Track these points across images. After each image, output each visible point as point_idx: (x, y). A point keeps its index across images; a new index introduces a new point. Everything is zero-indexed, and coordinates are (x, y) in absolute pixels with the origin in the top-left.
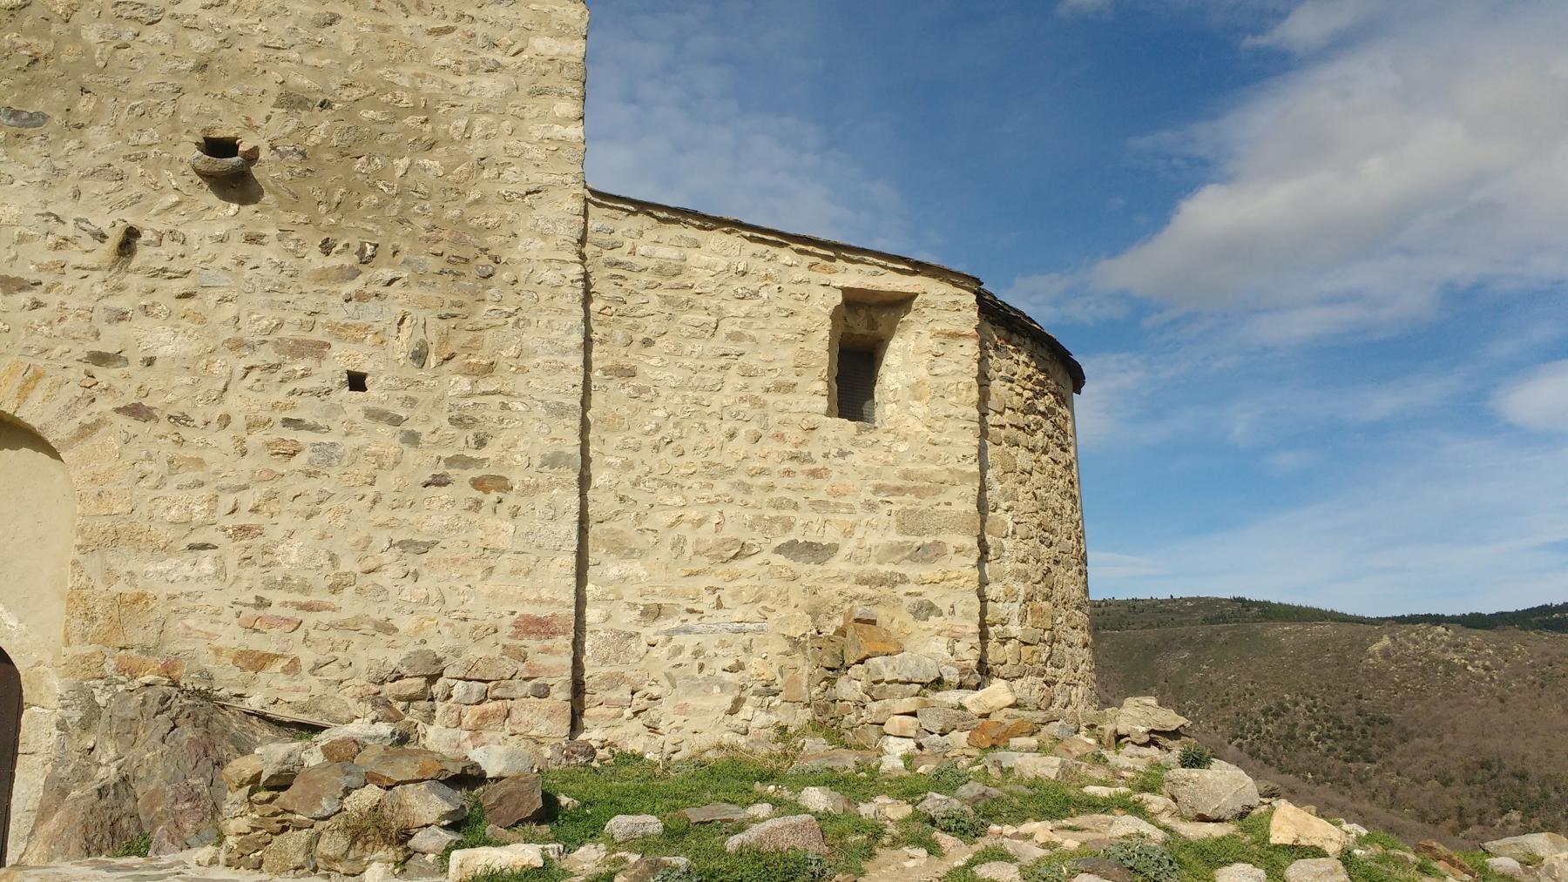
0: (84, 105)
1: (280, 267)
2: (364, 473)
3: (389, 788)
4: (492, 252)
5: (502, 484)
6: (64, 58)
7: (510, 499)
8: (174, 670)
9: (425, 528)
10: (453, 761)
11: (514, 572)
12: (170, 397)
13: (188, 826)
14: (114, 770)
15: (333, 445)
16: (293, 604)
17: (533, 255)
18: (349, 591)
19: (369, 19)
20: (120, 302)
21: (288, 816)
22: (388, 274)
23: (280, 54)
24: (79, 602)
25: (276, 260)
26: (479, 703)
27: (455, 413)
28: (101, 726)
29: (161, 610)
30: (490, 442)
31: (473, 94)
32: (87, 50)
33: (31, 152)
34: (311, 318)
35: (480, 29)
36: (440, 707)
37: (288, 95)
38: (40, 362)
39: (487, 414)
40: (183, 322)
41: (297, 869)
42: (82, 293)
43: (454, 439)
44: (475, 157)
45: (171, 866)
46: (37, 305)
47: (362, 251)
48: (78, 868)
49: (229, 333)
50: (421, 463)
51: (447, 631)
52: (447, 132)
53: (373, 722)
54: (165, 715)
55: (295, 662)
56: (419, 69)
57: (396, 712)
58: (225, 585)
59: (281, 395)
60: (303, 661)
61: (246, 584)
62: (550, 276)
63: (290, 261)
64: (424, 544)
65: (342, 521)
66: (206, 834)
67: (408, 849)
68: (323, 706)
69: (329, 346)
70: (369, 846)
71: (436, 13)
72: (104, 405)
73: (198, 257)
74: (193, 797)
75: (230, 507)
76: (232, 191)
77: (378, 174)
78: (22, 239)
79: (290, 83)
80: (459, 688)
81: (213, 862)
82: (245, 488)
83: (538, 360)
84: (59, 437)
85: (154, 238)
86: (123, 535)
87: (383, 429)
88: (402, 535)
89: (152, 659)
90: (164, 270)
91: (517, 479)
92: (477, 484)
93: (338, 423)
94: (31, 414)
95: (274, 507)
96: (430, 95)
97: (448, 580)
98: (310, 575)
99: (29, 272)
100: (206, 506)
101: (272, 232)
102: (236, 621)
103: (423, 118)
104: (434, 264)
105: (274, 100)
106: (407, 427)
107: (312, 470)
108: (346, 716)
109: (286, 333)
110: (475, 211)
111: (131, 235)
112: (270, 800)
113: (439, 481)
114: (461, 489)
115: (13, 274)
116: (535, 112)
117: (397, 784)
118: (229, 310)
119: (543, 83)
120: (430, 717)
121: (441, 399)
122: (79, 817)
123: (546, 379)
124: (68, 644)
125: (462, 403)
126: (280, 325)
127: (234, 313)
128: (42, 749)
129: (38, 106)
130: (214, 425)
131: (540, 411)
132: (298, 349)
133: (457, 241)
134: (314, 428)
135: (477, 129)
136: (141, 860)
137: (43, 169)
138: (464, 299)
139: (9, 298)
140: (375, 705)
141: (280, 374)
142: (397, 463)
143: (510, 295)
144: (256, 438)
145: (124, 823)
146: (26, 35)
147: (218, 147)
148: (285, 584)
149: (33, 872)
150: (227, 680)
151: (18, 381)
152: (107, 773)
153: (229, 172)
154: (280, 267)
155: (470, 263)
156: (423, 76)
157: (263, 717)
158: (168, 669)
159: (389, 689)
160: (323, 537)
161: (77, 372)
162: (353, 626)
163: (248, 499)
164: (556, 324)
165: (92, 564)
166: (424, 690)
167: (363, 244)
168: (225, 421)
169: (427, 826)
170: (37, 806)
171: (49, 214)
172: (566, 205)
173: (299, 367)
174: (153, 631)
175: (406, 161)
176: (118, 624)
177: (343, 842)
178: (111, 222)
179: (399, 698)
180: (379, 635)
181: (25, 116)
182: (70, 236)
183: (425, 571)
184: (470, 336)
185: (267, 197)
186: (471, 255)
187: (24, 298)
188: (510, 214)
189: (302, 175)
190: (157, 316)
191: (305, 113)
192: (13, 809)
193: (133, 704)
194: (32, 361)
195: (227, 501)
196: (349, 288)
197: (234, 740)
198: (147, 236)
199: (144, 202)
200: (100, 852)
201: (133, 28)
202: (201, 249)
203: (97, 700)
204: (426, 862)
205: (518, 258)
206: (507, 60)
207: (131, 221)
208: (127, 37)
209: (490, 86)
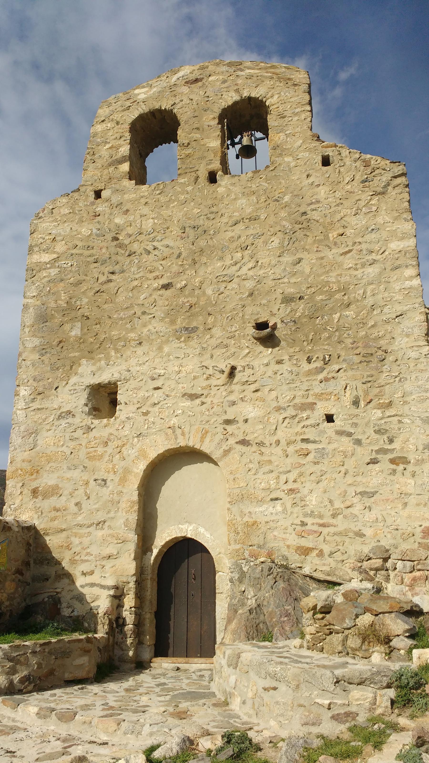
0: (210, 320)
1: (291, 372)
2: (339, 460)
3: (376, 615)
4: (383, 348)
5: (405, 461)
6: (201, 303)
7: (410, 468)
8: (272, 555)
9: (371, 485)
10: (406, 603)
11: (418, 505)
12: (256, 435)
13: (287, 628)
14: (254, 601)
15: (323, 449)
16: (317, 524)
17: (403, 346)
18: (340, 517)
19: (314, 256)
20: (232, 398)
21: (332, 627)
22: (337, 367)
23: (280, 281)
24: (231, 524)
25: (289, 369)
26: (411, 572)
27: (377, 428)
28: (246, 581)
29: (263, 528)
30: (395, 440)
31: (365, 277)
32: (209, 298)
33: (193, 343)
34: (307, 393)
35: (364, 246)
36: (392, 574)
37: (285, 298)
38: (207, 427)
39: (392, 426)
40: (257, 402)
41: (339, 653)
42: (218, 396)
43: (377, 440)
44: (369, 306)
45: (283, 647)
46: (203, 403)
47: (324, 359)
48: (246, 646)
49: (275, 404)
50: (364, 453)
51: (389, 536)
52: (355, 297)
53: (361, 581)
54: (271, 576)
55: (321, 551)
56: (339, 272)
57: (371, 576)
58: (288, 516)
59: (298, 429)
60: (325, 551)
61: (296, 515)
62: (413, 354)
63: (295, 369)
64: (371, 493)
65: (332, 484)
66: (295, 633)
67: (390, 647)
68: (337, 573)
69: (316, 404)
70: (371, 644)
71: (343, 245)
72: (232, 441)
73: (259, 374)
74: (288, 615)
75: (285, 481)
76: (268, 343)
77: (327, 323)
78: (195, 378)
79: (286, 292)
80: (400, 564)
81: (301, 647)
82: (289, 471)
83: (413, 397)
84: (217, 456)
85: (242, 369)
86: (245, 496)
87: (345, 439)
88: (360, 489)
89: (263, 551)
90: (247, 381)
91: (412, 457)
92: (392, 461)
93: (324, 438)
94: (206, 448)
95: (303, 479)
96: (345, 283)
97: (385, 510)
98: (322, 510)
99: (198, 391)
100: (275, 481)
101: (286, 357)
102: (294, 532)
103: (343, 293)
104: (357, 359)
105: (280, 301)
106: (355, 437)
107: (316, 461)
108: (348, 578)
109: (297, 401)
110: (373, 330)
111: (233, 368)
112: (323, 618)
113: (374, 462)
114: (385, 465)
115: (193, 392)
116: (395, 278)
117: (380, 613)
118: (274, 394)
119: (398, 263)
120: (387, 579)
121: (369, 422)
122: (243, 623)
123: (419, 406)
124: (230, 545)
125: (379, 422)
126: (294, 397)
127: (276, 395)
128: (225, 591)
129: (194, 324)
130: (274, 445)
131: (419, 422)
132: (303, 407)
133: (366, 346)
134: (314, 442)
135: (369, 293)
136: (270, 644)
137: (199, 349)
138: (373, 372)
139: (193, 402)
140: (361, 573)
141: (297, 419)
142: (353, 454)
143: (395, 368)
144: (291, 449)
145: (261, 625)
146: (187, 297)
147: (261, 326)
148: (312, 514)
149: (229, 647)
150: (294, 560)
151: (200, 435)
152: (251, 603)
153: (266, 334)
154: (291, 372)
155: (374, 355)
156: (341, 275)
157: (311, 578)
158: (269, 555)
159: (366, 565)
160: (325, 492)
161: (220, 429)
162: (344, 534)
163: (292, 477)
164: (420, 378)
165: (235, 509)
166: (383, 565)
167: (324, 356)
168: (278, 442)
169: (398, 636)
170: (226, 616)
171: (203, 366)
172: (417, 319)
173: (305, 415)
174: (261, 537)
175: (338, 314)
176: (248, 535)
177: (359, 641)
178: (225, 365)
179: (371, 569)
180: (357, 538)
181: (190, 329)
182: (211, 374)
183: (374, 506)
184: (378, 390)
185: (283, 343)
186: (373, 352)
187: (198, 401)
188: (389, 328)
189: (296, 331)
190: (246, 401)
191: (293, 304)
192: (217, 617)
193: (257, 571)
194: (204, 426)
195: (283, 478)
196: (321, 376)
197: (301, 588)
198: (239, 368)
199: (236, 354)
200: (253, 639)
201: (224, 285)
202: (260, 370)
203: (244, 569)
204: (400, 654)
205: (396, 349)
206: (379, 257)
207: (233, 363)
208: (222, 289)
209: (372, 271)
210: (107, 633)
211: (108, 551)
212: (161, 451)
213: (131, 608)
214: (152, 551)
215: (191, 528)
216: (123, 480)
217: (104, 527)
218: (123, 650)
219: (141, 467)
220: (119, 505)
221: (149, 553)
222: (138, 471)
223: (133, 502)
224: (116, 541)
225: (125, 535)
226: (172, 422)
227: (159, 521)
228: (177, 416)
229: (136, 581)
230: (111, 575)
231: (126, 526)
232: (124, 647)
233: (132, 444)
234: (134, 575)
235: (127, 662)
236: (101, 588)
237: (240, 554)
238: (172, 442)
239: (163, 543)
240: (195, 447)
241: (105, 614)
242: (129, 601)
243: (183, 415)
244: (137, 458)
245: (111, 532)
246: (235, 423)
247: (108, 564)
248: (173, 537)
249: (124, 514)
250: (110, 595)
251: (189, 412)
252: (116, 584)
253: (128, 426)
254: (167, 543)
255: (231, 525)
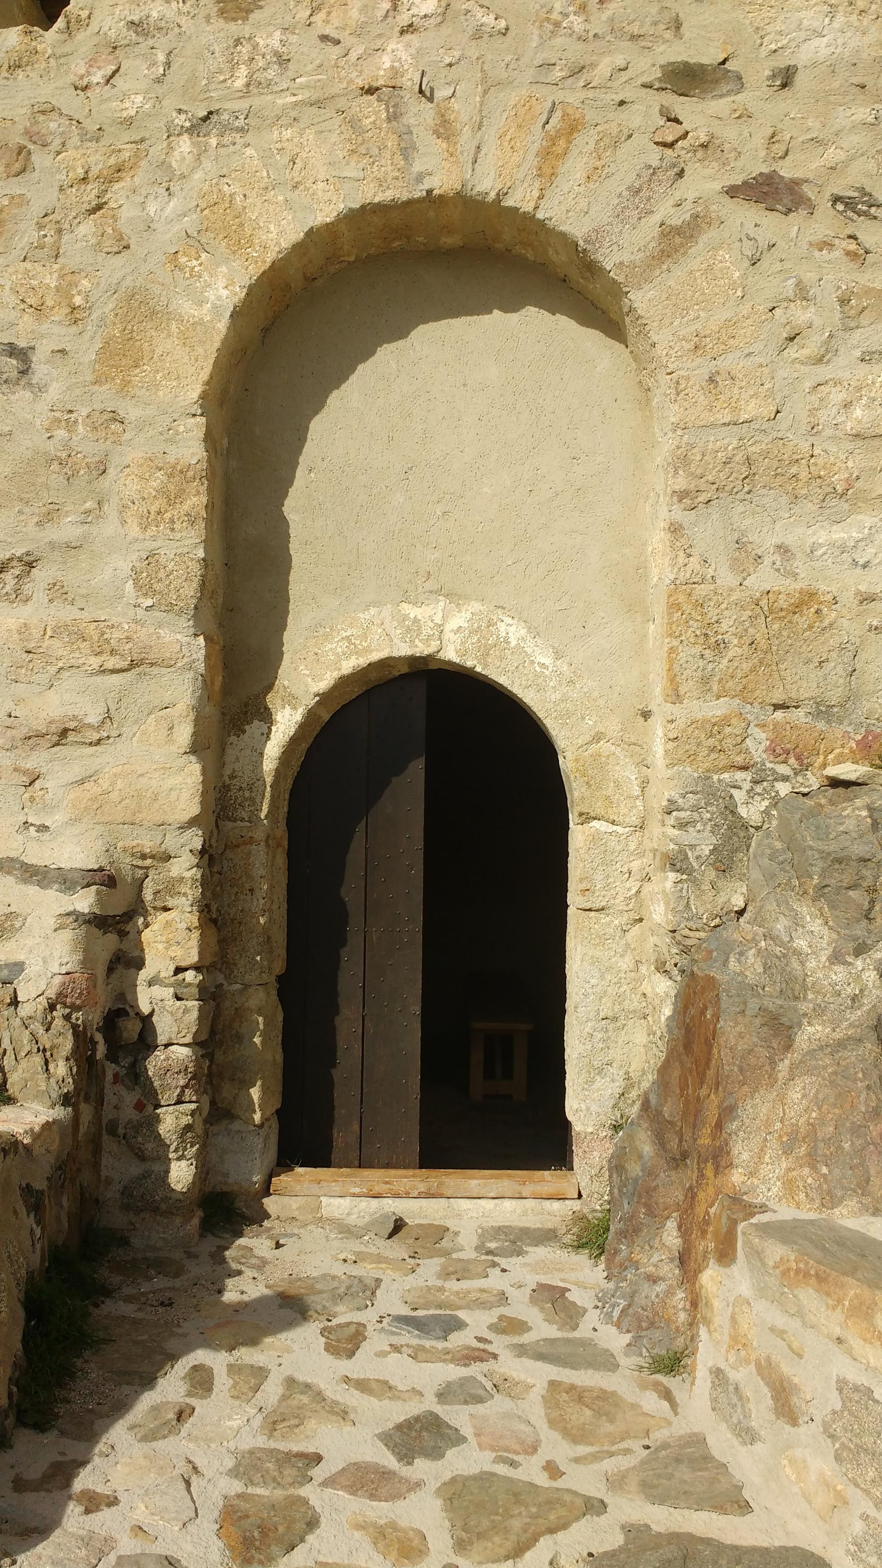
12: (833, 155)
29: (849, 628)
38: (573, 97)
72: (704, 182)
84: (626, 257)
89: (838, 730)
94: (572, 206)
151: (535, 140)
165: (708, 531)
174: (836, 670)
203: (743, 811)
210: (66, 1100)
211: (53, 705)
212: (325, 215)
213: (179, 970)
214: (267, 717)
215: (459, 620)
216: (121, 357)
217: (27, 588)
218: (143, 1158)
219: (218, 292)
220: (106, 482)
221: (255, 727)
222: (204, 312)
223: (177, 472)
224: (95, 662)
225: (143, 634)
226: (386, 61)
227: (298, 586)
228: (408, 29)
229: (203, 852)
230: (77, 820)
231: (144, 588)
232: (150, 1146)
233: (164, 165)
234: (193, 822)
235: (169, 1213)
236: (25, 881)
237: (729, 743)
238: (387, 166)
239: (324, 684)
240: (509, 202)
241: (52, 1007)
242: (170, 941)
243: (445, 30)
244: (194, 241)
245: (66, 614)
246: (724, 88)
247: (61, 769)
248: (375, 656)
249: (134, 530)
250: (75, 915)
251: (479, 13)
252: (104, 862)
253: (137, 71)
254: (343, 682)
255: (687, 608)
